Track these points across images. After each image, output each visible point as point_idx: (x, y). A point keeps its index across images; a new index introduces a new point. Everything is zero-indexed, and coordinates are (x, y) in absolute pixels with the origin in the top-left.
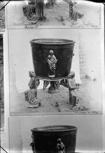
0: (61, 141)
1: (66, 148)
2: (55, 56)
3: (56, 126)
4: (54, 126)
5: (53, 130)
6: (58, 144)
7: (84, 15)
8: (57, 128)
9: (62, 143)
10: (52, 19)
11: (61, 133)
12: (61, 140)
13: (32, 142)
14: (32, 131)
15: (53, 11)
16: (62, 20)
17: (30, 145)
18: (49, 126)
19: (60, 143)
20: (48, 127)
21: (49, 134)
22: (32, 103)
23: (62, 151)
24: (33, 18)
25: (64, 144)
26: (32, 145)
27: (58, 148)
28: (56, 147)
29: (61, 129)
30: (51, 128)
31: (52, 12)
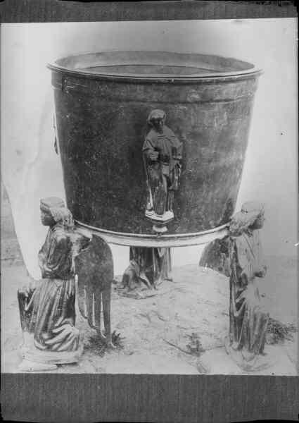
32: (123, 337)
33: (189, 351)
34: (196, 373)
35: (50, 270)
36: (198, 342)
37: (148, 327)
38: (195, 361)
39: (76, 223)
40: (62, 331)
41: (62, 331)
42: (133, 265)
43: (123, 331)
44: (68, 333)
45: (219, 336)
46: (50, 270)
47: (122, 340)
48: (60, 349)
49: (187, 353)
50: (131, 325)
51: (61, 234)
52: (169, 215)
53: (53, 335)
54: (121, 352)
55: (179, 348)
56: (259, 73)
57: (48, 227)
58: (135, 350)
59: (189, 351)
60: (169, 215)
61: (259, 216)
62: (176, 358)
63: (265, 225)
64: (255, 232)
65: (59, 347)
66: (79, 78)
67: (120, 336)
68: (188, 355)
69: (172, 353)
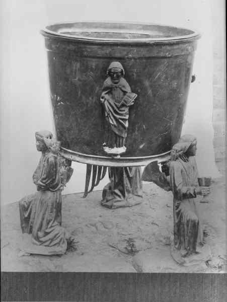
15: (101, 219)
31: (98, 225)
33: (127, 252)
34: (135, 271)
35: (44, 185)
36: (133, 245)
38: (131, 260)
39: (61, 149)
44: (56, 232)
46: (44, 185)
48: (50, 245)
50: (82, 232)
51: (51, 156)
53: (47, 234)
55: (119, 250)
56: (197, 37)
57: (41, 152)
59: (127, 252)
61: (191, 147)
63: (197, 152)
64: (191, 158)
65: (51, 242)
66: (75, 43)
67: (74, 241)
68: (127, 255)
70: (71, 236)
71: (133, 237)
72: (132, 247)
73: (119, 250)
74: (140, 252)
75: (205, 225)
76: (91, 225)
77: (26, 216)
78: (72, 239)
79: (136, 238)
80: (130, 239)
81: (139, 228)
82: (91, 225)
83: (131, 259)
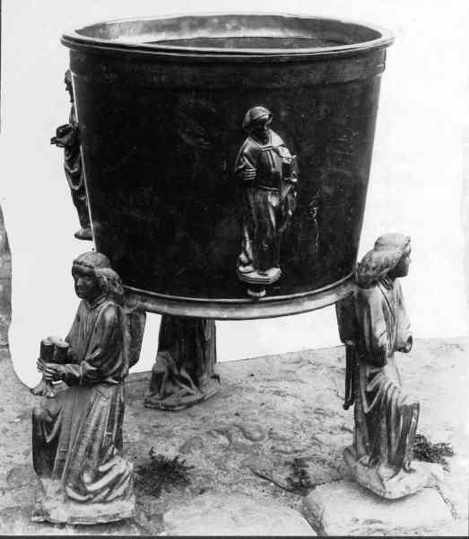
0: (271, 126)
1: (299, 176)
2: (244, 117)
3: (239, 18)
4: (223, 21)
5: (220, 43)
6: (250, 145)
7: (450, 454)
8: (243, 33)
9: (276, 140)
10: (227, 480)
11: (268, 71)
12: (274, 112)
13: (65, 121)
14: (67, 41)
15: (238, 420)
16: (300, 485)
17: (54, 141)
18: (192, 18)
19: (263, 138)
20: (185, 24)
21: (188, 71)
22: (91, 488)
23: (274, 194)
24: (112, 485)
25: (292, 142)
26: (65, 139)
27: (246, 167)
28: (231, 165)
29: (271, 42)
30: (203, 33)
31: (234, 431)
32: (190, 465)
36: (304, 473)
37: (228, 449)
40: (110, 469)
41: (110, 469)
42: (164, 357)
43: (190, 456)
45: (337, 464)
47: (188, 471)
48: (110, 498)
49: (288, 490)
52: (274, 273)
54: (187, 490)
55: (276, 484)
58: (207, 485)
60: (274, 273)
62: (269, 498)
64: (399, 280)
65: (110, 492)
69: (285, 496)
70: (177, 453)
71: (304, 455)
72: (301, 479)
73: (276, 484)
74: (318, 487)
75: (447, 433)
76: (218, 431)
77: (49, 439)
78: (180, 460)
79: (309, 459)
80: (296, 460)
81: (313, 438)
82: (218, 431)
83: (300, 502)
